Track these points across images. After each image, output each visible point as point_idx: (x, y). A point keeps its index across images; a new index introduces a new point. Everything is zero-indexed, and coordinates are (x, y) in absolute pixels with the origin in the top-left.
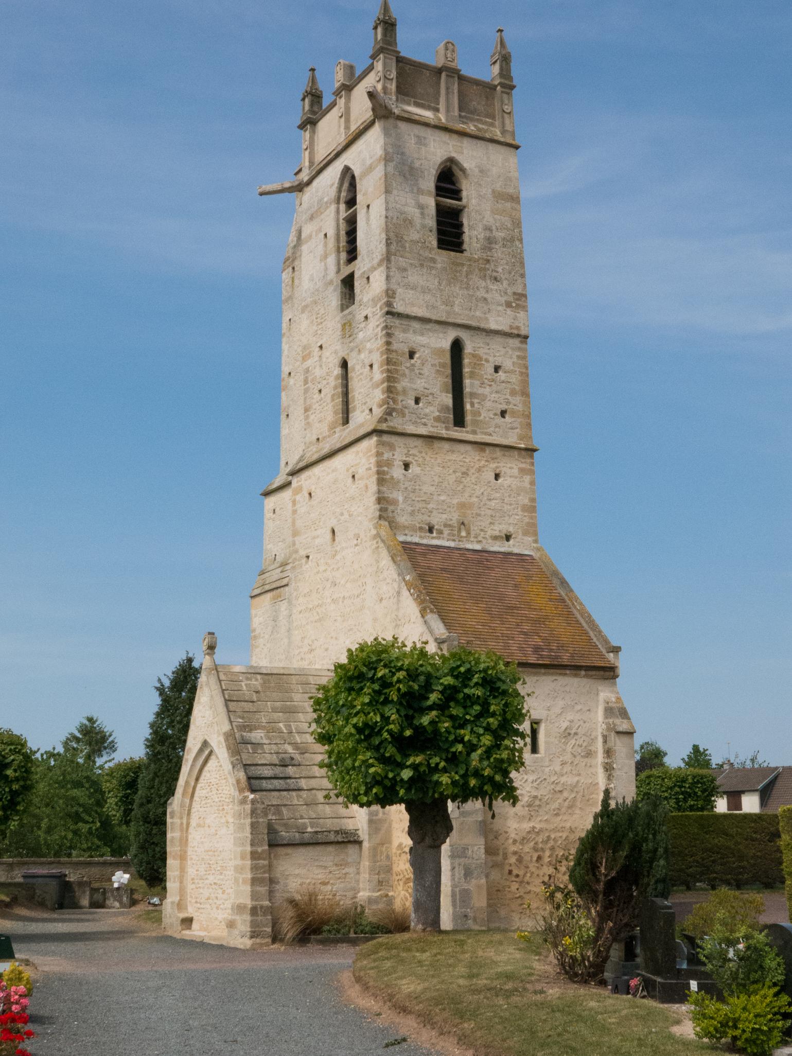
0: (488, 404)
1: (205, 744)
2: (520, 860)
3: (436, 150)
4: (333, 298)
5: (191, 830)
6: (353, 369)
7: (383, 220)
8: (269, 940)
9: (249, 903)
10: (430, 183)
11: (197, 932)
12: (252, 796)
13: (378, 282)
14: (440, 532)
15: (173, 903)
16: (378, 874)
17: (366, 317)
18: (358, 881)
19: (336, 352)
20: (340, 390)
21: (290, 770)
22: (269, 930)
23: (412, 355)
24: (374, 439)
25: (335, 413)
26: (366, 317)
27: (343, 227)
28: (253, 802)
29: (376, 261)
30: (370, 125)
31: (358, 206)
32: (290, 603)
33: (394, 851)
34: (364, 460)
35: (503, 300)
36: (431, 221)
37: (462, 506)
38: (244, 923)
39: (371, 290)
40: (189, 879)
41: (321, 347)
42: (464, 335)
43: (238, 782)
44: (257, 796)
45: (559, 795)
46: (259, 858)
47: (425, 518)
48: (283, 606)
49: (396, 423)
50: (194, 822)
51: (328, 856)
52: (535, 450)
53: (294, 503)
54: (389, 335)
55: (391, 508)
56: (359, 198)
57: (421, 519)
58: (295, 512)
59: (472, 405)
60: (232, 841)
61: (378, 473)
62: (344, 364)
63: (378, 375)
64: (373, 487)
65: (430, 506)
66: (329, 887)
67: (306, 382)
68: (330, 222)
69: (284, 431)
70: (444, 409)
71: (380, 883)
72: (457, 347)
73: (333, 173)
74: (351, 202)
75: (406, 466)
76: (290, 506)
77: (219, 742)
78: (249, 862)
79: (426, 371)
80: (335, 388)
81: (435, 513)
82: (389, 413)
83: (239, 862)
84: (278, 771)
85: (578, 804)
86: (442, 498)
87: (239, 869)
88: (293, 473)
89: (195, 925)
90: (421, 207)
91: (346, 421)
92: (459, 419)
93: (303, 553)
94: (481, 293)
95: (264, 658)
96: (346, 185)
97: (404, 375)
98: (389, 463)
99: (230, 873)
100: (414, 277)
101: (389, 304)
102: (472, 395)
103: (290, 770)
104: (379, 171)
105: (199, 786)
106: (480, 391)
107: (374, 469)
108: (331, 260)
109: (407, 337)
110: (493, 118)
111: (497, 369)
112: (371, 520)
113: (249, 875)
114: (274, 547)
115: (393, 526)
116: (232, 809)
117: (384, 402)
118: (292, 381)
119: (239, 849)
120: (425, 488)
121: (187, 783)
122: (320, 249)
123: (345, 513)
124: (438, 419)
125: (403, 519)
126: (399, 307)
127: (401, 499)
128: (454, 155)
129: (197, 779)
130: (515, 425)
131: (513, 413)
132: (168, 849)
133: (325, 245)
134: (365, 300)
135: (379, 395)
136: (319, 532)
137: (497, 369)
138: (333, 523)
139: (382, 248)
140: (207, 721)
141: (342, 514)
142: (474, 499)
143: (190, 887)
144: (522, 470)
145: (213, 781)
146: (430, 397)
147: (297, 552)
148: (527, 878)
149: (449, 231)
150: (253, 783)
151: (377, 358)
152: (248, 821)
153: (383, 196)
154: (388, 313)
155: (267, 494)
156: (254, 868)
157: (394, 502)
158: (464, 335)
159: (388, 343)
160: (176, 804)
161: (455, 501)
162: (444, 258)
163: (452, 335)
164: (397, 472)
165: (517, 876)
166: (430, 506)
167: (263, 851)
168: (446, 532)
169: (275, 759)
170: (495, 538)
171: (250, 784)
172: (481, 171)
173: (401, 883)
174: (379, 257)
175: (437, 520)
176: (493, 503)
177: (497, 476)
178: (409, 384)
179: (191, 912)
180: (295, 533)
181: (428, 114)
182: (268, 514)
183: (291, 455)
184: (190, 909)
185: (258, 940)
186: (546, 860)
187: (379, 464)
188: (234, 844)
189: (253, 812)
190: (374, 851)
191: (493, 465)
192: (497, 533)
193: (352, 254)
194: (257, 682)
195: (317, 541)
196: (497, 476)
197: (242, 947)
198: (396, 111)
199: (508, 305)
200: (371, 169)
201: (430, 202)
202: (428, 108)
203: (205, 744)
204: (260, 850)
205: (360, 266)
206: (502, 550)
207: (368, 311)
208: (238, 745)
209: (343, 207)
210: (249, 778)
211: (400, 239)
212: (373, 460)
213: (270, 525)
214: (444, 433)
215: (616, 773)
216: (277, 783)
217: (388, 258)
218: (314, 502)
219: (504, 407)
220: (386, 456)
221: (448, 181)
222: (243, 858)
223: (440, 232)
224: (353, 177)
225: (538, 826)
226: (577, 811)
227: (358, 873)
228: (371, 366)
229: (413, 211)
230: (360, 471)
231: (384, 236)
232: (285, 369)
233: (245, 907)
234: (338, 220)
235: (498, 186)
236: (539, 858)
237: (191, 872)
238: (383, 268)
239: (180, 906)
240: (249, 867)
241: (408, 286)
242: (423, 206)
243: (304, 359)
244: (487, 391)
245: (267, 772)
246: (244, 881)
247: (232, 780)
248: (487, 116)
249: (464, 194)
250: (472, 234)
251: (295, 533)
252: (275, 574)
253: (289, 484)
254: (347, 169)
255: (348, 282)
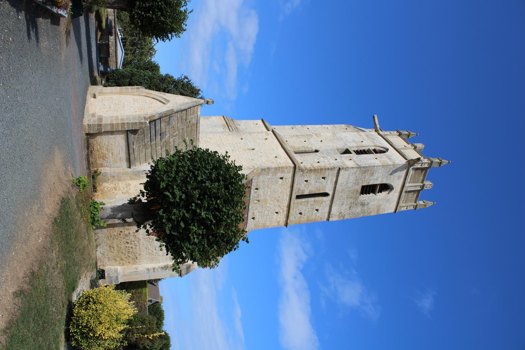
0: (304, 208)
1: (168, 101)
2: (126, 235)
3: (396, 182)
4: (343, 146)
5: (132, 96)
6: (316, 155)
7: (373, 165)
8: (87, 132)
9: (103, 123)
10: (385, 182)
11: (90, 100)
12: (148, 122)
13: (350, 164)
14: (256, 193)
15: (102, 90)
16: (118, 176)
17: (336, 159)
18: (114, 167)
19: (321, 147)
20: (307, 149)
21: (158, 137)
22: (92, 132)
23: (324, 178)
24: (293, 165)
25: (298, 148)
26: (336, 159)
27: (366, 149)
28: (146, 123)
29: (358, 163)
30: (406, 159)
31: (375, 154)
32: (223, 132)
33: (128, 182)
34: (283, 161)
35: (343, 211)
36: (372, 183)
37: (266, 201)
38: (93, 121)
39: (349, 161)
40: (112, 96)
41: (321, 141)
42: (330, 198)
43: (154, 116)
44: (148, 124)
45: (154, 248)
46: (122, 127)
47: (262, 187)
48: (221, 130)
49: (298, 175)
50: (135, 97)
51: (123, 155)
52: (286, 226)
53: (262, 132)
54: (331, 169)
55: (265, 173)
56: (379, 155)
57: (261, 185)
58: (258, 133)
59: (304, 202)
60: (128, 114)
61: (279, 168)
62: (317, 151)
63: (316, 165)
64: (273, 166)
65: (266, 188)
66: (111, 156)
67: (307, 135)
68: (368, 144)
69: (287, 127)
70: (303, 191)
71: (114, 177)
72: (326, 195)
73: (388, 146)
74: (376, 151)
75: (281, 178)
76: (260, 131)
77: (169, 107)
78: (120, 122)
79: (318, 184)
80: (307, 147)
81: (263, 190)
82: (302, 171)
83: (120, 118)
84: (158, 133)
85: (151, 256)
86: (269, 193)
87: (117, 118)
88: (273, 131)
89: (93, 99)
90: (377, 179)
91: (296, 153)
92: (298, 197)
93: (243, 137)
94: (345, 203)
95: (204, 123)
96: (385, 150)
97: (316, 176)
98: (283, 172)
99: (115, 114)
100: (352, 178)
101: (343, 168)
102: (308, 202)
103: (158, 137)
104: (390, 163)
105: (150, 99)
106: (309, 205)
107: (280, 166)
108: (354, 144)
109: (331, 177)
110: (405, 203)
111: (317, 210)
112: (260, 165)
113: (114, 122)
114: (243, 124)
115: (260, 174)
116: (142, 113)
117: (306, 169)
118: (306, 129)
119: (125, 117)
120: (273, 186)
121: (151, 94)
122: (357, 140)
123: (262, 154)
124: (299, 189)
125: (261, 178)
126: (342, 172)
127: (269, 177)
128: (394, 189)
129: (153, 98)
130: (296, 219)
131: (300, 217)
132: (124, 87)
133: (359, 142)
134: (343, 159)
135: (308, 166)
136: (252, 143)
137: (317, 210)
138: (257, 149)
139: (363, 165)
140: (177, 101)
141: (261, 153)
142: (268, 205)
143: (108, 96)
144: (279, 222)
145: (153, 105)
146: (307, 186)
147: (243, 134)
148: (119, 238)
149: (367, 189)
150: (153, 122)
151: (322, 165)
152: (137, 121)
153: (381, 164)
154: (340, 169)
155: (262, 121)
156: (117, 124)
157: (268, 174)
158: (330, 198)
159: (328, 169)
160: (143, 90)
161: (268, 198)
162: (359, 190)
163: (331, 193)
164: (280, 175)
165: (120, 235)
166: (266, 188)
167: (124, 128)
168: (256, 195)
169: (163, 130)
170: (253, 214)
171: (152, 121)
172: (388, 200)
173: (114, 186)
174: (359, 164)
175: (261, 191)
176: (267, 212)
177: (277, 213)
178: (312, 178)
179: (99, 97)
180: (250, 133)
181: (408, 179)
182: (255, 121)
183: (278, 129)
184: (99, 97)
185: (87, 128)
186: (127, 245)
187: (282, 168)
188: (127, 116)
189: (142, 123)
190: (127, 174)
191: (281, 211)
192: (255, 214)
193: (359, 152)
194: (194, 121)
195: (249, 143)
196: (277, 213)
197: (84, 121)
198: (411, 168)
199: (341, 213)
200: (390, 159)
201: (379, 182)
202: (410, 179)
203: (168, 101)
204: (125, 126)
205: (354, 155)
206: (249, 217)
207: (339, 160)
208: (168, 116)
209: (373, 148)
210: (155, 120)
211: (365, 172)
212: (284, 165)
213: (251, 123)
214: (294, 192)
215: (164, 271)
216: (153, 132)
217: (359, 167)
218: (264, 141)
219: (303, 214)
220: (286, 170)
221: (385, 187)
222: (122, 119)
223: (367, 186)
224: (384, 152)
225: (141, 242)
226: (148, 256)
227: (117, 167)
228: (318, 162)
229: (376, 176)
230: (279, 160)
231: (368, 165)
232: (309, 126)
233: (101, 121)
234: (368, 146)
235: (382, 207)
236: (128, 243)
237: (115, 97)
238: (356, 166)
239: (101, 93)
240: (118, 122)
241: (349, 175)
242: (377, 180)
243: (316, 135)
244: (309, 207)
245: (158, 127)
246: (112, 120)
247: (154, 113)
248: (406, 200)
249: (380, 194)
250: (366, 197)
251: (250, 133)
252: (233, 126)
253: (268, 130)
254: (387, 150)
255: (347, 152)
